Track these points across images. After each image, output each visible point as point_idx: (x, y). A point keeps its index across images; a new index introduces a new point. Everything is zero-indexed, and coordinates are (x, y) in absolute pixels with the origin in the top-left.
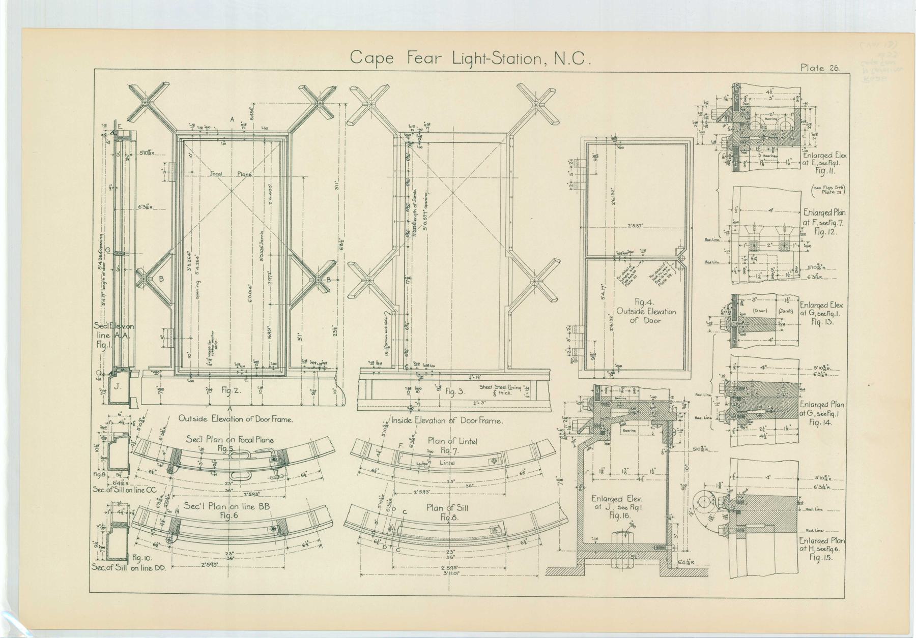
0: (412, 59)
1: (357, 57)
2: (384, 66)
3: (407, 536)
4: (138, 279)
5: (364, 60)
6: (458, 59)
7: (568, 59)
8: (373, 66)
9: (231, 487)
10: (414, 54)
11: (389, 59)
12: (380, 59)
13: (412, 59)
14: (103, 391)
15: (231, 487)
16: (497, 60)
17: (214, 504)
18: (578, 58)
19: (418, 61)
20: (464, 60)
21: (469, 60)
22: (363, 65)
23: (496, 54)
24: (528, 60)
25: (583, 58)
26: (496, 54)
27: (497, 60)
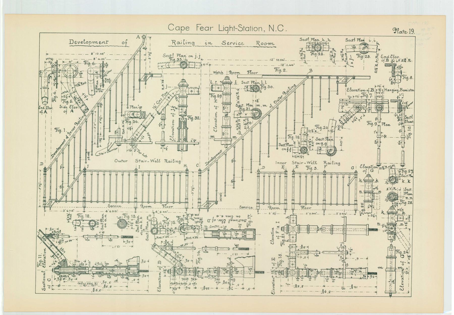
0: (199, 28)
1: (171, 27)
2: (185, 32)
5: (175, 29)
7: (276, 29)
8: (179, 32)
10: (200, 26)
11: (187, 28)
12: (183, 28)
13: (199, 28)
18: (281, 28)
20: (224, 29)
21: (227, 29)
22: (175, 31)
23: (240, 26)
25: (283, 28)
26: (240, 26)
27: (241, 29)
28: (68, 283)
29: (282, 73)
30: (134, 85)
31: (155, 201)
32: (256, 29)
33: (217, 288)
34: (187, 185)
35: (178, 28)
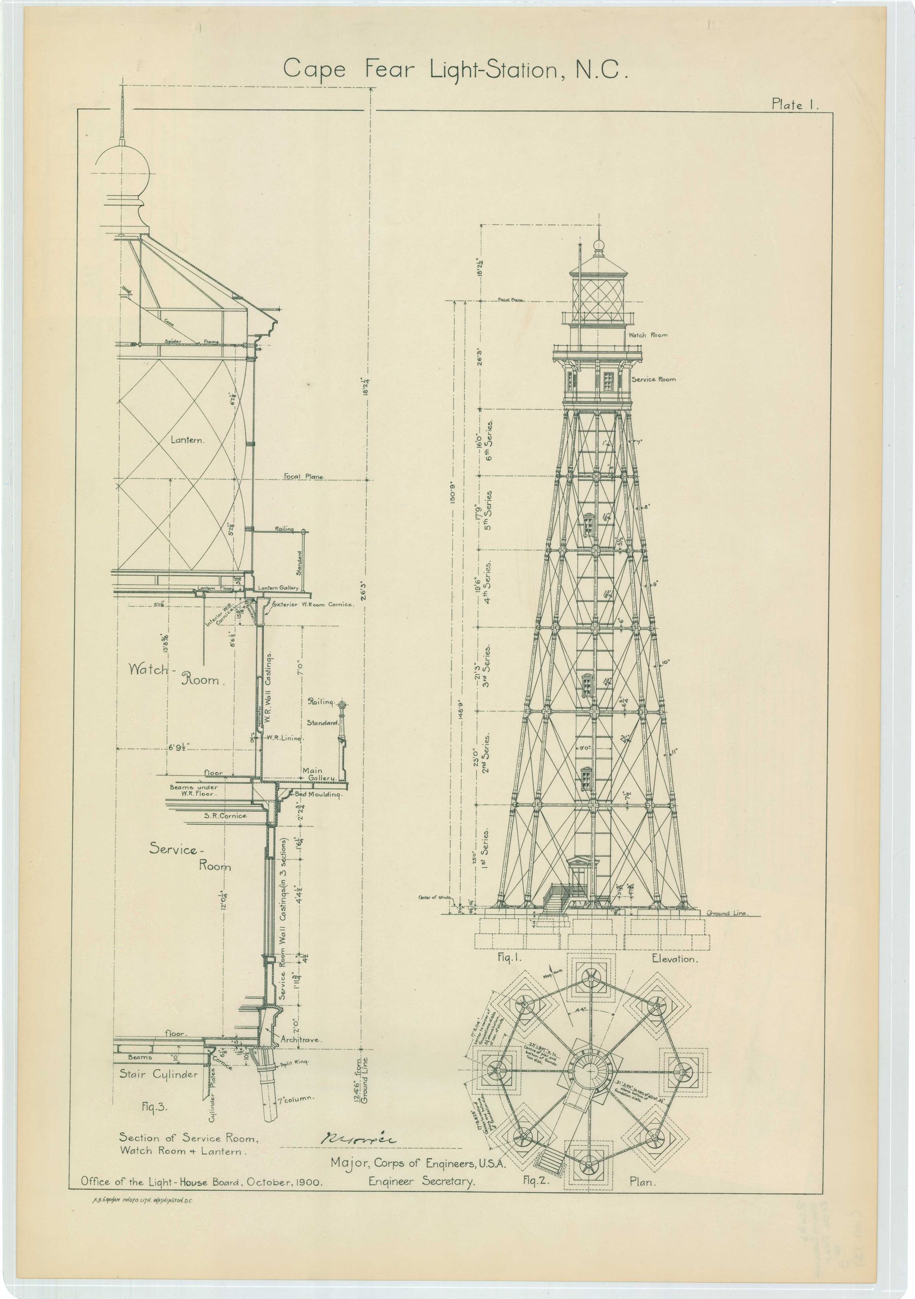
0: (372, 70)
1: (292, 67)
2: (332, 80)
3: (190, 592)
4: (155, 313)
5: (303, 72)
6: (438, 71)
7: (596, 70)
8: (316, 80)
9: (465, 903)
11: (339, 70)
12: (326, 71)
13: (372, 70)
14: (214, 815)
15: (465, 903)
16: (495, 72)
17: (637, 1179)
18: (610, 69)
19: (380, 73)
20: (446, 72)
21: (453, 71)
22: (302, 79)
23: (492, 63)
24: (538, 72)
25: (617, 69)
26: (492, 63)
27: (495, 72)
28: (582, 925)
29: (540, 1187)
30: (123, 131)
31: (596, 582)
32: (538, 72)
33: (361, 1049)
34: (248, 811)
35: (311, 71)
